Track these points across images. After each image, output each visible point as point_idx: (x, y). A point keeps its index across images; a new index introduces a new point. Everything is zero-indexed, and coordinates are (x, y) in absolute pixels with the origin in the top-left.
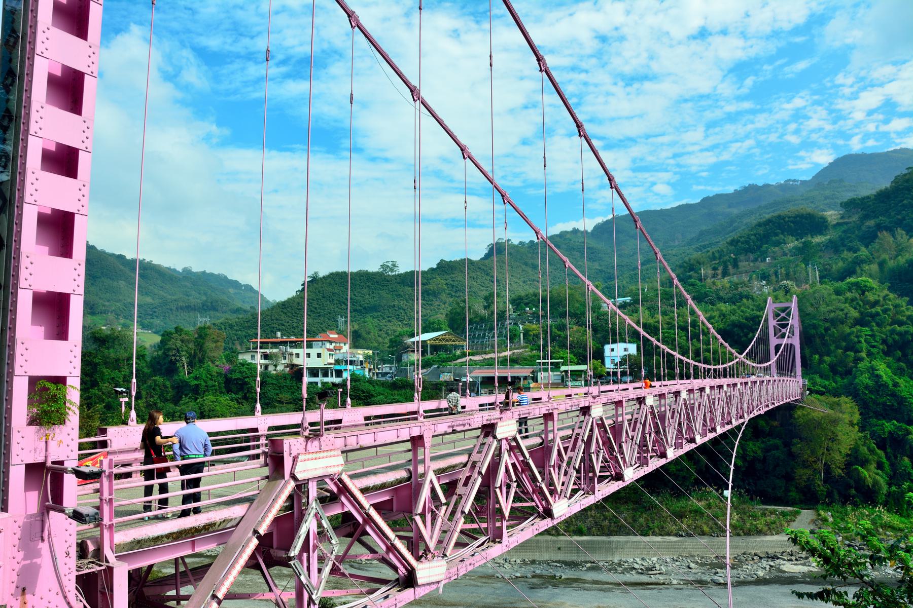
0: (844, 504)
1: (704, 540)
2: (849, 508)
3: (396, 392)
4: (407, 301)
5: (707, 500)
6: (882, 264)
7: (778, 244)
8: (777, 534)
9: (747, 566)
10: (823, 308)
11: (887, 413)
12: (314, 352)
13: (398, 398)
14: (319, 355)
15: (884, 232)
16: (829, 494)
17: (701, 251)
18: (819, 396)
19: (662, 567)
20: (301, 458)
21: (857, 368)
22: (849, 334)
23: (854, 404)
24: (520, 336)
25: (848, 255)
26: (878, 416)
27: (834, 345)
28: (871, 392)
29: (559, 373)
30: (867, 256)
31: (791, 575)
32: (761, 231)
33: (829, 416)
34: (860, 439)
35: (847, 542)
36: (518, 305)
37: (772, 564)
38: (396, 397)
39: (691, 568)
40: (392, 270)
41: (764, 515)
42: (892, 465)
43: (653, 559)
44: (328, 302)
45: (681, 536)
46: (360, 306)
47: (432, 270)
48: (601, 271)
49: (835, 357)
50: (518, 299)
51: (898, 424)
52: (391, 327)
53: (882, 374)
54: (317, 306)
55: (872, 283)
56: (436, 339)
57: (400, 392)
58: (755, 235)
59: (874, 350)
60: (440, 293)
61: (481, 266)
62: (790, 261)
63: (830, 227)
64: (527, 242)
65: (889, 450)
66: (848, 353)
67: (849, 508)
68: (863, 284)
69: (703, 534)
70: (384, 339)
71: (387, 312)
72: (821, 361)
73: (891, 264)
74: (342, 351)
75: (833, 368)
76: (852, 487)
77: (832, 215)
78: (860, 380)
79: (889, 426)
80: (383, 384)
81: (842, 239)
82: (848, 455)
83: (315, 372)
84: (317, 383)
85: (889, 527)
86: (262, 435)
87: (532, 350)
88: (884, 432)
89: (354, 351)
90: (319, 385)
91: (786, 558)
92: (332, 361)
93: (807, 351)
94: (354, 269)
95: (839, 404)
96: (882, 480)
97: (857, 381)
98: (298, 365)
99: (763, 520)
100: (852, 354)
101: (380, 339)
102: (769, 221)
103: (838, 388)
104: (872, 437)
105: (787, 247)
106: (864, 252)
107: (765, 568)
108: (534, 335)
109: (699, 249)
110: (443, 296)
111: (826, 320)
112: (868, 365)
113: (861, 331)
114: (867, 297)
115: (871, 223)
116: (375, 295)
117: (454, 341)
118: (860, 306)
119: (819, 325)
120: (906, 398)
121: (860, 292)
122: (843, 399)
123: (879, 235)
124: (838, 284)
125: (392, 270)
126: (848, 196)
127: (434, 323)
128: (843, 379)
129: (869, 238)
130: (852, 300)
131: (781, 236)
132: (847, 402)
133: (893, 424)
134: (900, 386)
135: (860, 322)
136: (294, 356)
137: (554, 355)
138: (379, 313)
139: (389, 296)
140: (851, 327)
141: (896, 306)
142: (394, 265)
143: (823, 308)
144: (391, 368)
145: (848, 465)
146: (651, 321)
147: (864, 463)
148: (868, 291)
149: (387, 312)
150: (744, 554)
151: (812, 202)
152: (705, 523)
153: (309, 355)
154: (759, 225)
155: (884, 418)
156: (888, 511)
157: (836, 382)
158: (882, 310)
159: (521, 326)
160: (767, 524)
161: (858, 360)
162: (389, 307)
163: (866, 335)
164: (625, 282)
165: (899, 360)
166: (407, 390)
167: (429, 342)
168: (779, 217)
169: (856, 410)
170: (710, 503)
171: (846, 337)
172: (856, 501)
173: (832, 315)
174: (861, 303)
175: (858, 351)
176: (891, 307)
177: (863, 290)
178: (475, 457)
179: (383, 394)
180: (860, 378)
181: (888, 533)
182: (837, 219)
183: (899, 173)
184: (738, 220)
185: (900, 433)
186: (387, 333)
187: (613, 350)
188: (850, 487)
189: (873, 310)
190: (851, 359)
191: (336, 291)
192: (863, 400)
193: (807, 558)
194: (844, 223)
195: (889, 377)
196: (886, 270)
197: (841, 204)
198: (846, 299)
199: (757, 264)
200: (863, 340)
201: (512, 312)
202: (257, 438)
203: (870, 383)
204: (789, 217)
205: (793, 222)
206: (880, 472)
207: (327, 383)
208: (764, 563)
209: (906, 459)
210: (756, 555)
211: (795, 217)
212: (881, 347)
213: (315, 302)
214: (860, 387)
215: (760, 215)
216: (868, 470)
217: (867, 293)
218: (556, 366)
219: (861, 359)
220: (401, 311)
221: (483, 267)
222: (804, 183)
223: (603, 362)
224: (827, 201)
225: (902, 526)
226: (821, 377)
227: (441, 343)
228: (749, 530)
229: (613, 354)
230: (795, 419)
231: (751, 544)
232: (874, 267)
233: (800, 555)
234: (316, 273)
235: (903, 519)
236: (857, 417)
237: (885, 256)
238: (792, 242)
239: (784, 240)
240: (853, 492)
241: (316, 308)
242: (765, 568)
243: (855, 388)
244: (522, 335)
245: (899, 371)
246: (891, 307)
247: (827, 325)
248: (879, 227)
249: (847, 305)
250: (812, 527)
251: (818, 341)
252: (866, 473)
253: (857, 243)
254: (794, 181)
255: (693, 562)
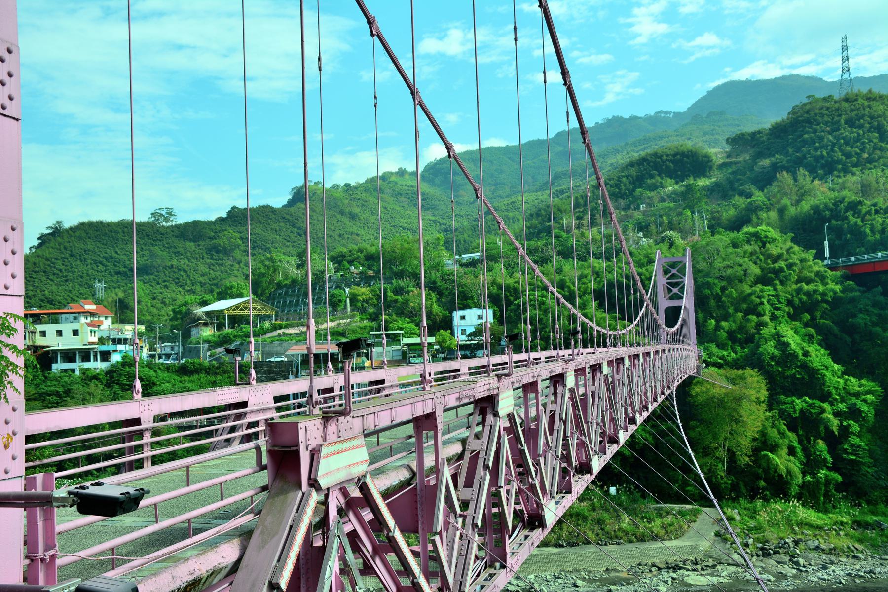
0: (752, 498)
1: (591, 549)
2: (759, 503)
3: (187, 378)
4: (189, 260)
5: (590, 499)
6: (782, 211)
7: (653, 188)
8: (676, 538)
9: (644, 580)
10: (718, 264)
11: (798, 388)
12: (67, 327)
13: (189, 385)
14: (76, 333)
15: (785, 173)
16: (734, 487)
17: (558, 197)
18: (716, 369)
19: (542, 587)
20: (325, 451)
21: (760, 334)
22: (750, 294)
23: (761, 377)
24: (346, 302)
25: (741, 202)
26: (789, 392)
27: (732, 308)
28: (778, 363)
29: (398, 348)
30: (763, 202)
31: (698, 588)
32: (633, 171)
33: (732, 391)
34: (767, 419)
35: (760, 545)
36: (340, 263)
37: (674, 575)
38: (187, 385)
39: (577, 586)
40: (167, 220)
41: (660, 516)
42: (805, 450)
43: (530, 577)
44: (79, 262)
45: (562, 546)
46: (125, 267)
47: (221, 219)
48: (435, 222)
49: (734, 321)
50: (341, 256)
51: (810, 401)
52: (169, 294)
53: (790, 341)
54: (62, 268)
55: (773, 233)
56: (237, 307)
57: (192, 378)
58: (627, 177)
59: (778, 313)
60: (232, 250)
61: (285, 215)
62: (670, 209)
63: (715, 168)
64: (342, 185)
65: (801, 433)
66: (750, 317)
67: (759, 503)
68: (763, 234)
69: (587, 542)
70: (159, 310)
71: (162, 275)
72: (718, 327)
73: (792, 211)
74: (102, 327)
75: (731, 334)
76: (760, 478)
77: (717, 152)
78: (765, 350)
79: (799, 403)
80: (168, 368)
81: (731, 183)
82: (754, 439)
83: (70, 355)
84: (73, 371)
85: (806, 524)
86: (147, 430)
87: (362, 319)
88: (795, 412)
89: (120, 326)
90: (78, 373)
91: (690, 568)
92: (95, 340)
93: (700, 315)
94: (253, 204)
95: (743, 378)
96: (795, 466)
97: (761, 349)
98: (44, 347)
99: (658, 522)
100: (754, 318)
101: (154, 311)
102: (643, 161)
103: (738, 359)
104: (780, 417)
105: (664, 192)
106: (759, 197)
107: (666, 582)
108: (364, 301)
109: (556, 195)
110: (237, 254)
111: (721, 278)
112: (774, 331)
113: (762, 291)
114: (768, 249)
115: (766, 162)
116: (144, 252)
117: (259, 310)
118: (761, 260)
119: (714, 284)
120: (819, 370)
121: (760, 244)
122: (749, 371)
123: (778, 176)
124: (734, 235)
125: (167, 220)
126: (734, 131)
127: (232, 287)
128: (743, 348)
129: (765, 180)
130: (752, 254)
131: (658, 178)
132: (752, 376)
133: (804, 401)
134: (810, 356)
135: (763, 280)
136: (38, 335)
137: (391, 325)
138: (152, 277)
139: (165, 253)
140: (751, 286)
141: (803, 261)
142: (170, 213)
143: (718, 264)
144: (172, 348)
145: (756, 451)
146: (510, 281)
147: (774, 448)
148: (769, 242)
149: (162, 275)
150: (640, 564)
151: (689, 139)
152: (590, 529)
153: (60, 333)
154: (632, 164)
155: (793, 395)
156: (803, 505)
157: (736, 353)
158: (786, 266)
159: (347, 290)
160: (663, 527)
161: (760, 325)
162: (165, 268)
163: (769, 295)
164: (466, 236)
165: (806, 325)
166: (202, 376)
167: (226, 312)
168: (655, 155)
169: (763, 386)
170: (594, 504)
171: (746, 298)
172: (766, 495)
173: (729, 271)
174: (761, 257)
175: (759, 315)
176: (798, 262)
177: (763, 241)
178: (473, 445)
179: (169, 382)
180: (765, 347)
181: (805, 531)
182: (723, 158)
183: (798, 103)
184: (602, 160)
185: (813, 411)
186: (163, 303)
187: (463, 318)
188: (758, 478)
189: (777, 266)
190: (753, 324)
191: (90, 247)
192: (768, 372)
193: (714, 566)
194: (731, 163)
195: (798, 345)
196: (786, 217)
197: (727, 140)
198: (745, 252)
199: (631, 212)
200: (765, 302)
201: (332, 273)
202: (140, 434)
203: (777, 353)
204: (667, 156)
205: (671, 161)
206: (791, 458)
207: (88, 369)
208: (665, 575)
209: (821, 442)
210: (653, 565)
211: (675, 155)
212: (787, 309)
213: (60, 262)
214: (766, 358)
215: (628, 153)
216: (779, 457)
217: (768, 245)
218: (393, 339)
219: (764, 324)
220: (182, 273)
221: (287, 217)
222: (677, 115)
223: (452, 334)
224: (707, 138)
225: (820, 523)
226: (718, 346)
227: (242, 313)
228: (644, 535)
229: (463, 322)
230: (691, 396)
231: (646, 552)
232: (773, 215)
233: (706, 564)
234: (59, 223)
235: (820, 514)
236: (764, 394)
237: (786, 201)
238: (671, 185)
239: (661, 183)
240: (762, 483)
241: (61, 271)
242: (666, 582)
243: (759, 358)
244: (348, 300)
245: (807, 338)
246: (798, 262)
247: (724, 283)
248: (776, 168)
249: (746, 259)
250: (717, 528)
251: (713, 303)
252: (778, 460)
253: (750, 187)
254: (667, 113)
255: (580, 579)
